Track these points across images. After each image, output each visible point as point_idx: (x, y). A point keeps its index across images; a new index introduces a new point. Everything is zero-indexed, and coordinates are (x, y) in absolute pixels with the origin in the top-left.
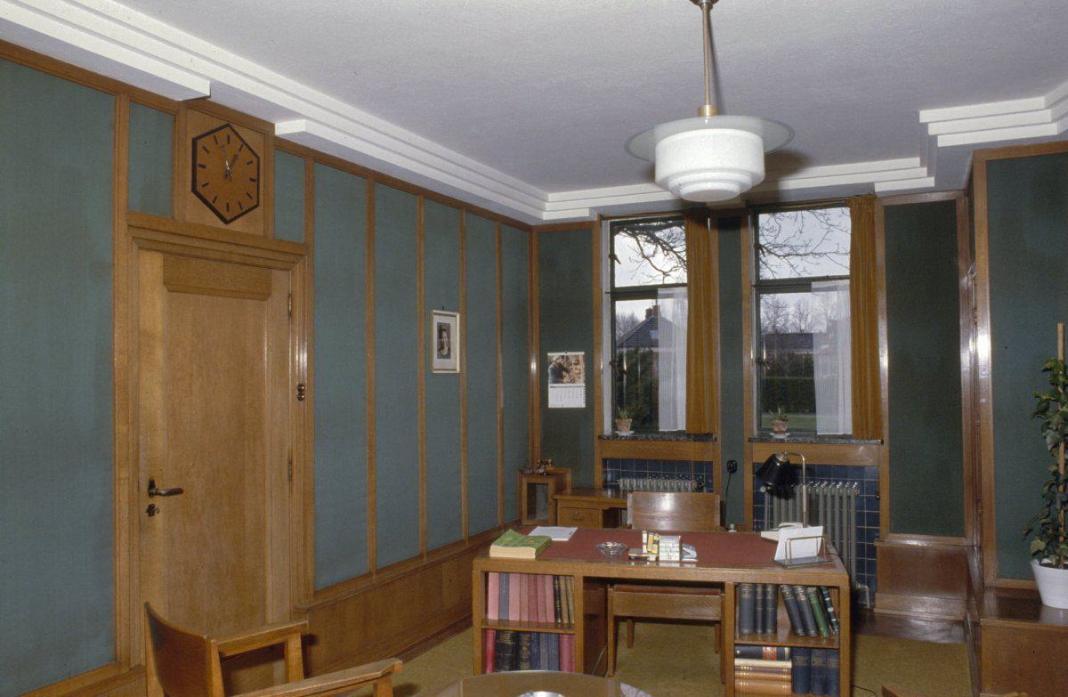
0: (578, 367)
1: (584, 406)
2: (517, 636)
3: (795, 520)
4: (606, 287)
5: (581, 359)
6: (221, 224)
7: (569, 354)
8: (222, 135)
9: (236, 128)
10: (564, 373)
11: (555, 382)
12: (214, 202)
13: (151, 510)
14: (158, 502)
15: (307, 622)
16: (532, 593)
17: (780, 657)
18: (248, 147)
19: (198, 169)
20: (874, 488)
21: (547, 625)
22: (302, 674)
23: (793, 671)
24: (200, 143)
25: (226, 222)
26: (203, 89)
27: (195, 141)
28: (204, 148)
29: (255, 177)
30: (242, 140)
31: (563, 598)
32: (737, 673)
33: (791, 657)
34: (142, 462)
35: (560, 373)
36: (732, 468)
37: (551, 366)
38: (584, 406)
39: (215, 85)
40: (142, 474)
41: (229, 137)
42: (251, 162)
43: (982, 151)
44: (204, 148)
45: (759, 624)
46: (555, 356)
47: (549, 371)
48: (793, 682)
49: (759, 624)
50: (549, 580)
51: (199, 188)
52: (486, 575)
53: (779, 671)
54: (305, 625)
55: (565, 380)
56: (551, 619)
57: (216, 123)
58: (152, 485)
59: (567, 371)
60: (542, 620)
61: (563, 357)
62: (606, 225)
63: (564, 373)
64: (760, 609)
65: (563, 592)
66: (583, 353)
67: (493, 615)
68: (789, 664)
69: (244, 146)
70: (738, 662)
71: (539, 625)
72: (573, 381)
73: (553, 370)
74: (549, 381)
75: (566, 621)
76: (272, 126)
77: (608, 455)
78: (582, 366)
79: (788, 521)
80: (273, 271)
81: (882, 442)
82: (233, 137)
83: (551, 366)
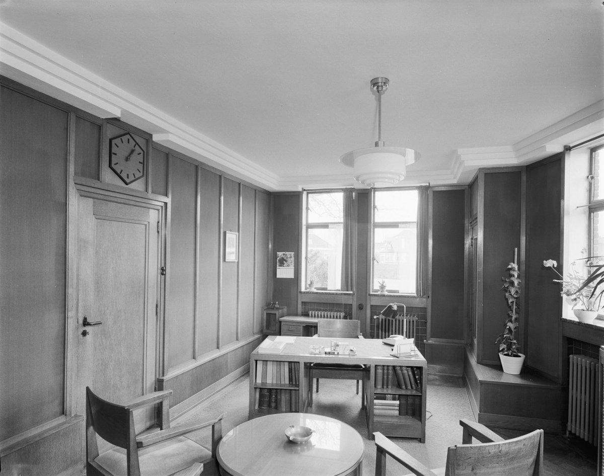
0: (291, 259)
1: (293, 277)
2: (270, 390)
3: (399, 334)
4: (304, 222)
5: (293, 255)
6: (123, 185)
7: (287, 253)
8: (125, 138)
9: (133, 135)
10: (284, 262)
11: (280, 266)
12: (121, 173)
13: (84, 333)
14: (88, 329)
15: (172, 391)
16: (278, 370)
17: (394, 399)
18: (139, 146)
19: (113, 155)
20: (424, 317)
21: (285, 385)
22: (154, 390)
23: (400, 405)
24: (114, 142)
25: (127, 184)
26: (117, 113)
27: (111, 141)
28: (116, 144)
29: (142, 161)
30: (135, 141)
31: (293, 372)
32: (375, 407)
33: (399, 399)
34: (80, 308)
35: (282, 262)
36: (361, 307)
37: (278, 258)
38: (293, 277)
39: (124, 112)
40: (80, 315)
41: (129, 140)
42: (115, 164)
43: (483, 169)
44: (116, 144)
45: (385, 384)
46: (280, 254)
47: (277, 261)
48: (399, 410)
49: (385, 384)
50: (287, 365)
51: (113, 166)
52: (256, 361)
53: (393, 405)
54: (171, 393)
55: (284, 265)
56: (287, 382)
57: (122, 132)
58: (85, 319)
59: (286, 261)
60: (283, 383)
61: (284, 254)
62: (305, 193)
63: (284, 262)
64: (385, 377)
65: (293, 369)
66: (293, 253)
67: (259, 381)
68: (397, 402)
69: (137, 145)
70: (376, 401)
71: (281, 385)
72: (288, 266)
73: (279, 260)
74: (278, 265)
75: (294, 383)
76: (151, 136)
77: (304, 300)
78: (293, 259)
79: (395, 334)
80: (150, 210)
81: (429, 297)
82: (131, 140)
83: (278, 258)
